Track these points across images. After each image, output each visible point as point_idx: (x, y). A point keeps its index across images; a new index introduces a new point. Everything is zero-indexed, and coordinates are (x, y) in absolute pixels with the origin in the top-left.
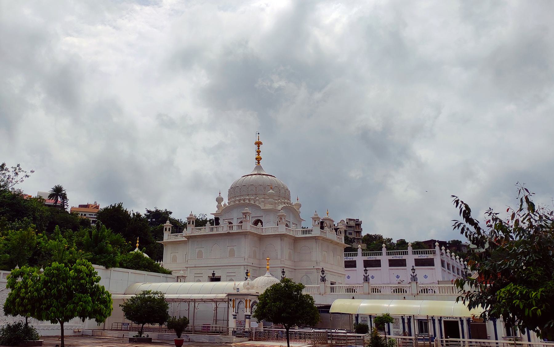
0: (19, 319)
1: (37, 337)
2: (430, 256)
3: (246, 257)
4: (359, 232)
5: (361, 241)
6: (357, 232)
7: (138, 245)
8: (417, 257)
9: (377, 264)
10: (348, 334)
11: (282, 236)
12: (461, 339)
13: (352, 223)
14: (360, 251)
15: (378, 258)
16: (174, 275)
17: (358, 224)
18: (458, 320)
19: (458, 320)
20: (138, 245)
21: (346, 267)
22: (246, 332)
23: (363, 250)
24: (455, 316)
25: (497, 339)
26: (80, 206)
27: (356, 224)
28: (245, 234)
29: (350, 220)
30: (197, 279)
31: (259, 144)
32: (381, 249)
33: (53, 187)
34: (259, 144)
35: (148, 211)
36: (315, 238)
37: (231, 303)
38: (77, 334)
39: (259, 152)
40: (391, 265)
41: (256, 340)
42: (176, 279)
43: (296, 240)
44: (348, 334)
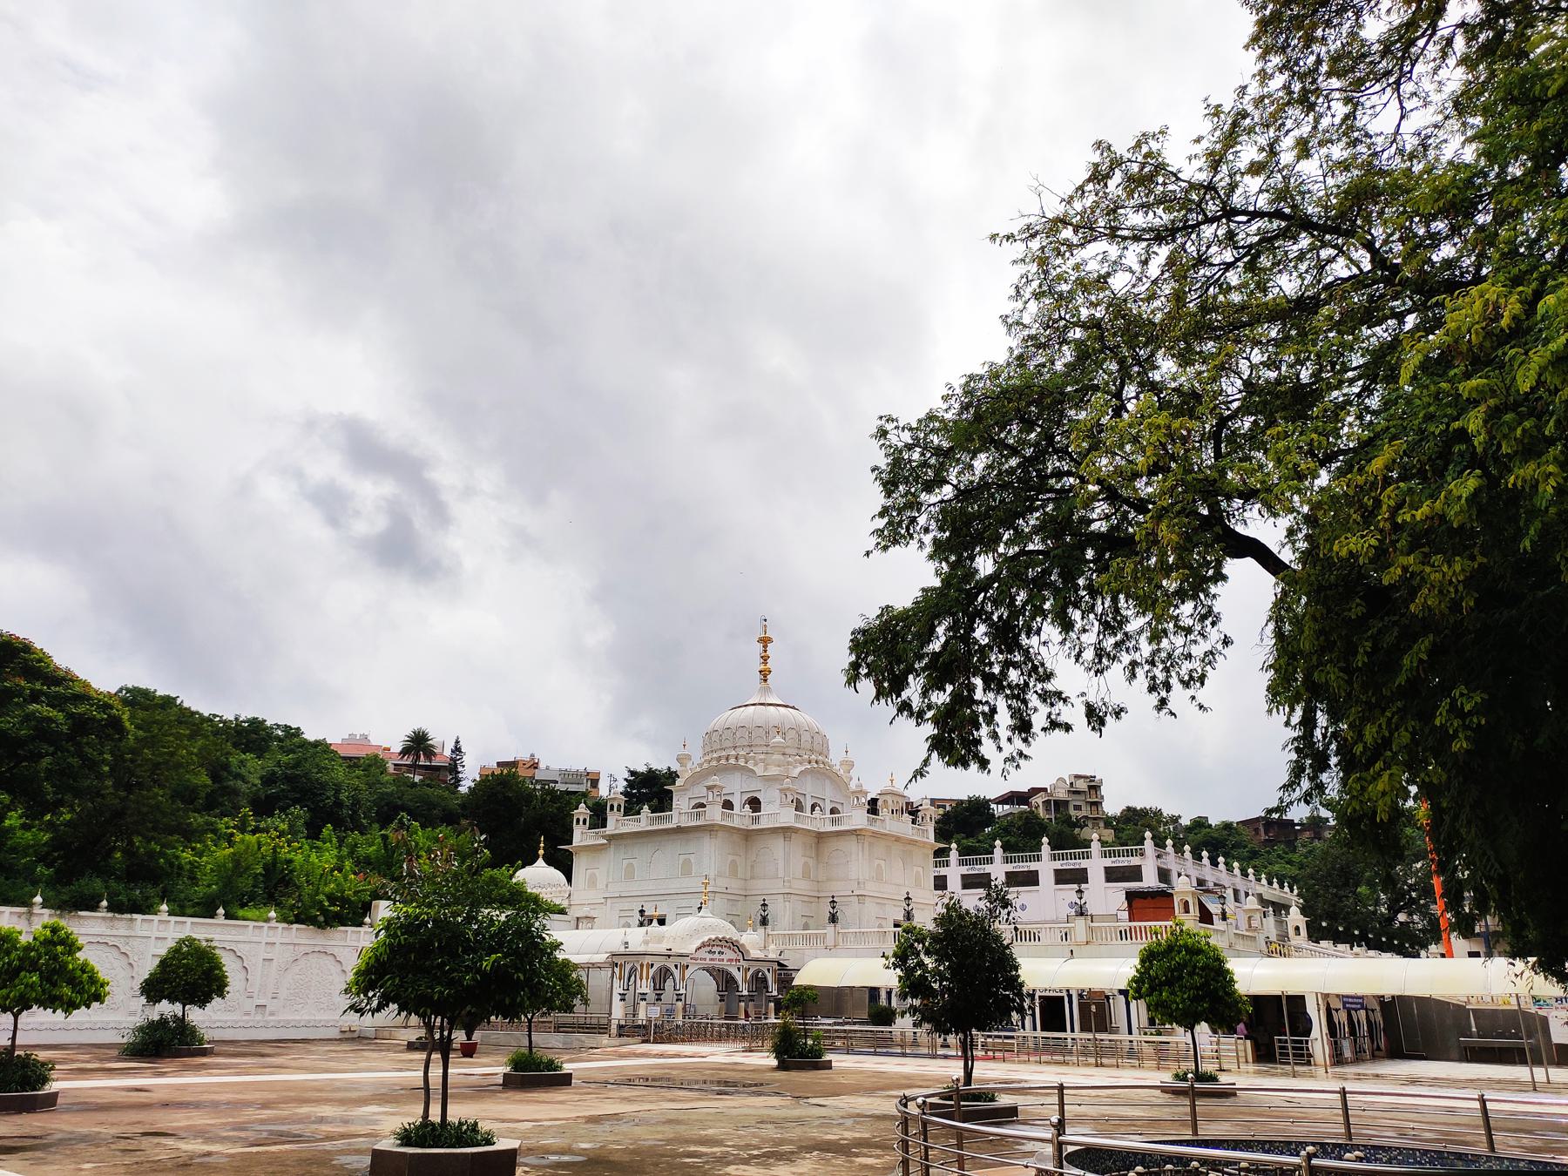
0: (166, 1008)
1: (201, 1041)
2: (1135, 861)
3: (712, 876)
4: (1097, 804)
5: (1102, 824)
6: (1092, 804)
7: (541, 852)
8: (1058, 865)
9: (1031, 879)
10: (847, 1027)
11: (786, 832)
12: (1068, 1034)
13: (1082, 785)
14: (1095, 847)
15: (1033, 866)
16: (574, 912)
17: (1095, 787)
18: (1064, 994)
19: (1064, 994)
20: (541, 852)
21: (1057, 883)
22: (639, 1026)
23: (1104, 843)
24: (1057, 986)
25: (1130, 1033)
26: (499, 764)
27: (1090, 787)
28: (710, 829)
29: (1077, 777)
30: (623, 921)
31: (765, 641)
32: (1142, 841)
33: (846, 641)
34: (765, 641)
35: (633, 773)
36: (855, 833)
37: (617, 970)
38: (347, 1035)
39: (765, 659)
40: (1108, 880)
41: (655, 1042)
42: (574, 923)
43: (820, 837)
44: (847, 1027)
